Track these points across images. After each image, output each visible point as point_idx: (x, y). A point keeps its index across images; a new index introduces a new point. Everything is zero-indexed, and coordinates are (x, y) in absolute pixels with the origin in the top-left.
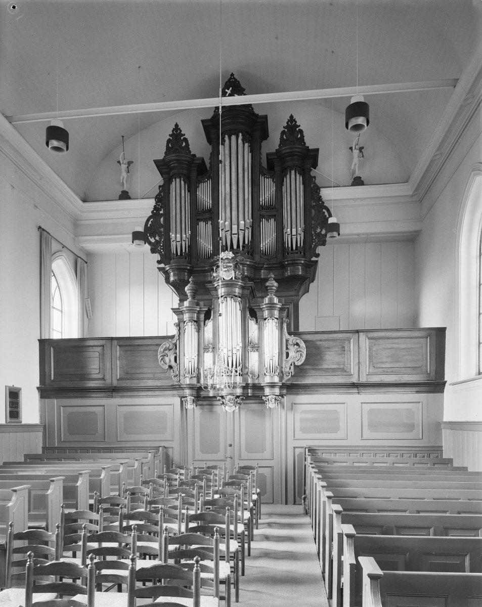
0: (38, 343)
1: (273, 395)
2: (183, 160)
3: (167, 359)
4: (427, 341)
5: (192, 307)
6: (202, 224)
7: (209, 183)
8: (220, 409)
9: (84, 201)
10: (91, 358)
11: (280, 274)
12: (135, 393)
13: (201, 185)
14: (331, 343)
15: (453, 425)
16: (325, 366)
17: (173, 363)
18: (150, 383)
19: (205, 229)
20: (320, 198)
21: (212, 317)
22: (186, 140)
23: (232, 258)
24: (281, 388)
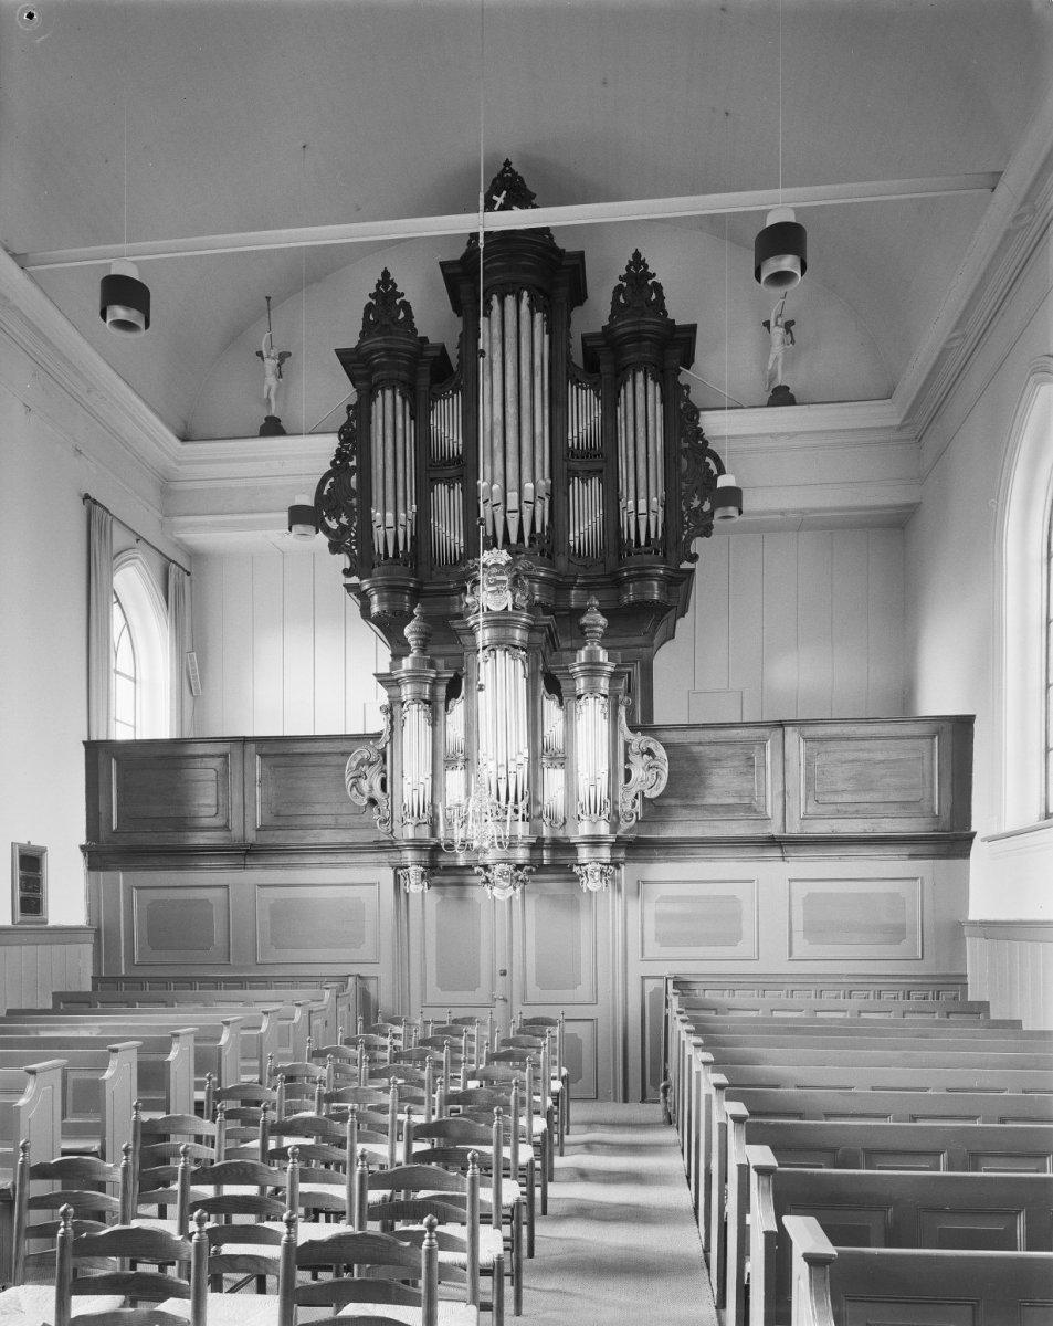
0: (82, 749)
1: (597, 862)
2: (399, 350)
3: (365, 785)
4: (933, 744)
5: (420, 671)
6: (441, 489)
7: (458, 399)
8: (480, 894)
9: (184, 439)
10: (199, 781)
11: (612, 598)
12: (296, 859)
13: (440, 405)
14: (723, 750)
15: (990, 929)
16: (711, 800)
17: (378, 794)
18: (328, 837)
19: (447, 499)
20: (699, 433)
21: (463, 693)
22: (406, 306)
23: (508, 564)
24: (614, 847)
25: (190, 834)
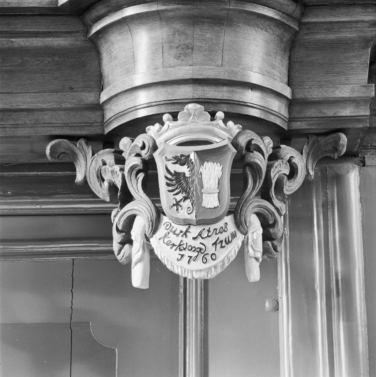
1: (210, 106)
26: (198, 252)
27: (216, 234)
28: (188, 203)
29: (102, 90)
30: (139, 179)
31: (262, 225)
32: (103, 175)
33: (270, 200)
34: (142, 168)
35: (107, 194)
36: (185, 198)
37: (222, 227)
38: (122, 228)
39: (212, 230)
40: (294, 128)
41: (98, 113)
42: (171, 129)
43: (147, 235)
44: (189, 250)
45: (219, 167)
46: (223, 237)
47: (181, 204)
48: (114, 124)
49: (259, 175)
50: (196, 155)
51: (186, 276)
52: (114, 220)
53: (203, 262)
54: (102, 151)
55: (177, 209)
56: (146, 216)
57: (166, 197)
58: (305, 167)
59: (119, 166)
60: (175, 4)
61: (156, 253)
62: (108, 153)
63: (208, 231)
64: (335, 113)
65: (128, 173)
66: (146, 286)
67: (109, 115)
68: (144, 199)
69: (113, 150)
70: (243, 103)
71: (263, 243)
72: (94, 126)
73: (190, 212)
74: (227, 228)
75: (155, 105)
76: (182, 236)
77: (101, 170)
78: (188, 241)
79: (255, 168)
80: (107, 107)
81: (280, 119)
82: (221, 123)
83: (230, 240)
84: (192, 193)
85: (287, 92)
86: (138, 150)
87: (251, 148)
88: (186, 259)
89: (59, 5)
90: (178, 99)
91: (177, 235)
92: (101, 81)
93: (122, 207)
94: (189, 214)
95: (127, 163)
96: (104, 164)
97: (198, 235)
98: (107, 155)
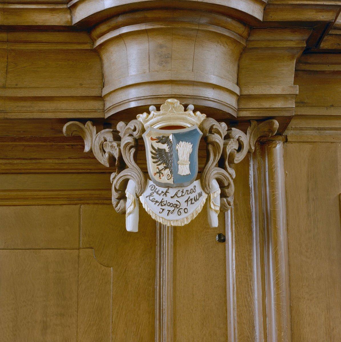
1: (185, 101)
25: (274, 164)
26: (175, 207)
27: (188, 194)
28: (167, 171)
29: (104, 87)
30: (131, 153)
31: (220, 187)
32: (104, 148)
33: (225, 168)
34: (133, 145)
35: (107, 162)
36: (166, 168)
37: (192, 189)
38: (119, 188)
39: (185, 191)
40: (241, 116)
41: (101, 103)
42: (155, 117)
43: (138, 194)
44: (168, 205)
45: (190, 145)
46: (192, 196)
47: (163, 172)
48: (112, 111)
49: (218, 150)
50: (173, 136)
51: (166, 224)
52: (113, 182)
53: (179, 215)
54: (104, 130)
55: (160, 176)
56: (137, 180)
57: (152, 167)
58: (249, 144)
59: (116, 143)
60: (159, 24)
61: (144, 207)
62: (107, 132)
63: (182, 192)
64: (270, 106)
65: (123, 148)
66: (136, 230)
67: (108, 105)
68: (135, 168)
69: (111, 130)
70: (207, 99)
71: (220, 200)
72: (97, 112)
73: (169, 178)
74: (195, 190)
75: (143, 99)
76: (163, 195)
77: (103, 144)
78: (168, 199)
79: (215, 145)
80: (107, 99)
81: (232, 110)
82: (191, 113)
83: (198, 198)
84: (171, 164)
85: (237, 90)
86: (131, 132)
87: (212, 131)
88: (166, 212)
89: (73, 24)
90: (161, 95)
91: (160, 194)
92: (102, 79)
93: (119, 172)
94: (168, 179)
95: (122, 140)
96: (106, 140)
97: (174, 195)
98: (107, 134)
